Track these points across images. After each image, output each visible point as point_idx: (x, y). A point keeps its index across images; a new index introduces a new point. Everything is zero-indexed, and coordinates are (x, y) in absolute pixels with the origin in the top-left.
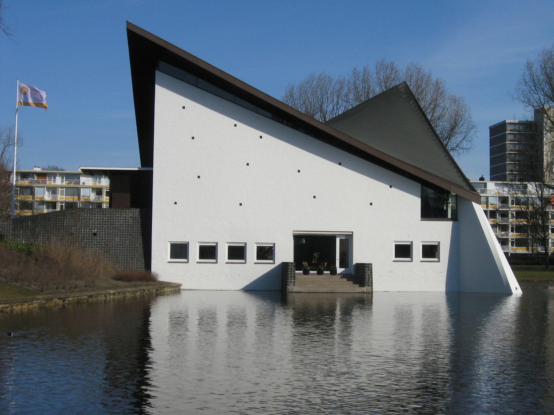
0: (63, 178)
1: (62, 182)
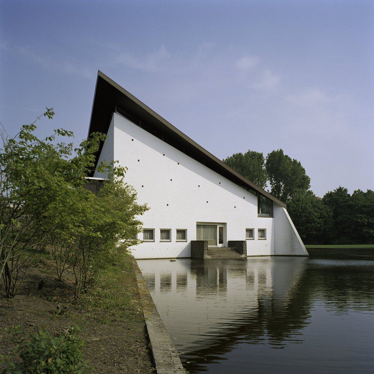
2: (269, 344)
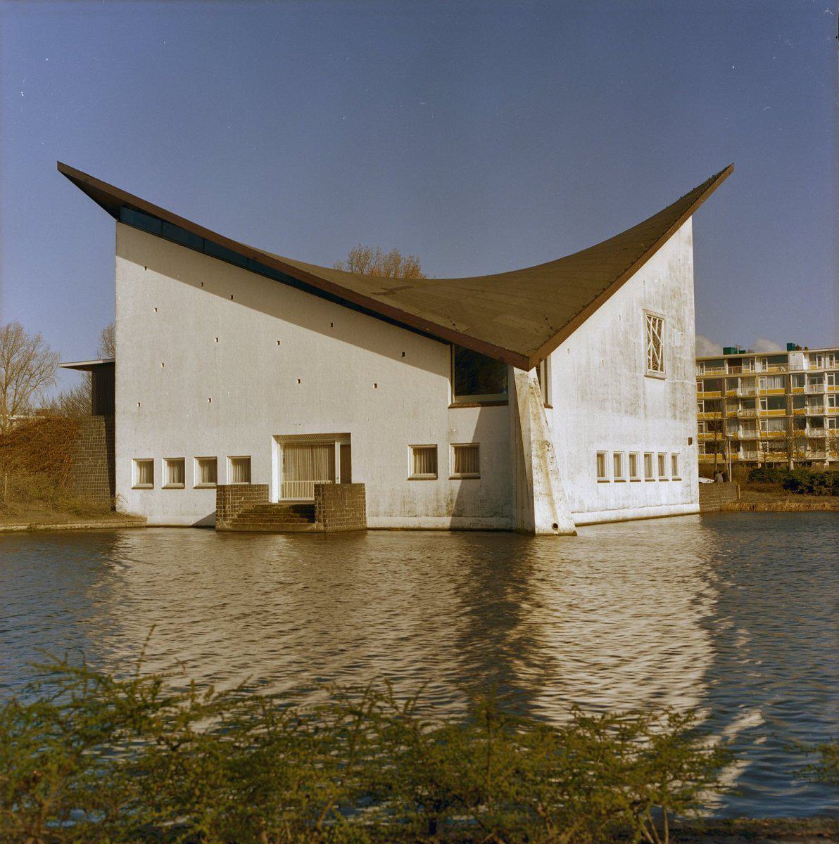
0: (764, 363)
1: (831, 364)
2: (451, 479)
